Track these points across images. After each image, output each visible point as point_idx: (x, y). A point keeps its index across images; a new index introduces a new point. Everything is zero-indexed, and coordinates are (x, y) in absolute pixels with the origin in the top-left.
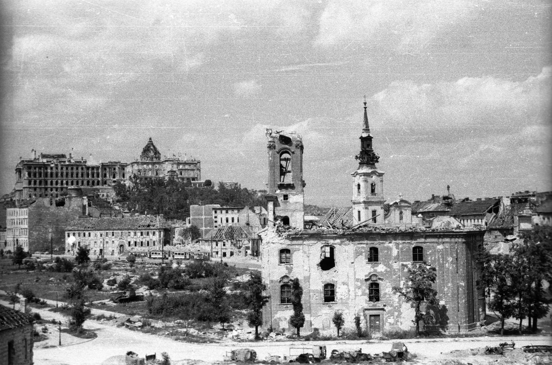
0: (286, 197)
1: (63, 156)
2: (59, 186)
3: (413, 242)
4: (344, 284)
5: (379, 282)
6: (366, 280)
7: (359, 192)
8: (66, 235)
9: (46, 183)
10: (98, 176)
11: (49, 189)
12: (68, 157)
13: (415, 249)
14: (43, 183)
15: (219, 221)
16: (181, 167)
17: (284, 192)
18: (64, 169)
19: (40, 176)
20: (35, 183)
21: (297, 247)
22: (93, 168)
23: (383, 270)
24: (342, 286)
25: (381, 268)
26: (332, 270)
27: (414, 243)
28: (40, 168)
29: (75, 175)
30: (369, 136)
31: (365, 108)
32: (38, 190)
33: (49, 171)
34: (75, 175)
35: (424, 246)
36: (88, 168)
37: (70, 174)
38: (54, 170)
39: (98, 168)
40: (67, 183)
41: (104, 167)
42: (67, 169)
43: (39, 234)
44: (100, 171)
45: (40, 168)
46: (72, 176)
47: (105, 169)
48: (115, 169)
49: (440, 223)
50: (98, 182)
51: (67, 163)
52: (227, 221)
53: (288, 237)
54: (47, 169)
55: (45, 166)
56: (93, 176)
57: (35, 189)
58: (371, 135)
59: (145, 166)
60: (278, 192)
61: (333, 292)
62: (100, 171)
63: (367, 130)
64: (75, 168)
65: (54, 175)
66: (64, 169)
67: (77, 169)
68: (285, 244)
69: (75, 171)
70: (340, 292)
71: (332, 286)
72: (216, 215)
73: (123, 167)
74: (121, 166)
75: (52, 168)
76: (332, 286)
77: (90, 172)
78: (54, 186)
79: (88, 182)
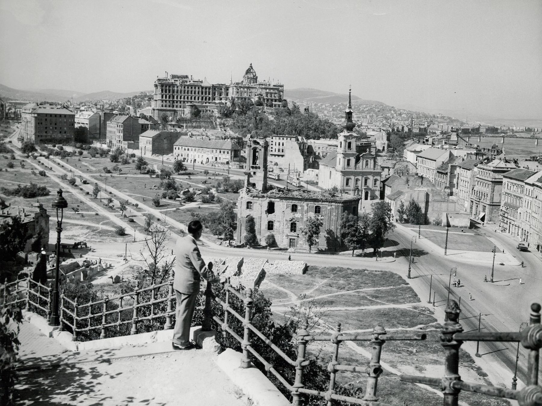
0: (255, 173)
1: (187, 77)
2: (182, 100)
3: (316, 203)
4: (279, 222)
5: (296, 222)
6: (290, 221)
7: (341, 147)
8: (174, 149)
9: (173, 97)
10: (209, 94)
11: (175, 102)
12: (190, 77)
13: (316, 207)
14: (171, 97)
15: (274, 143)
16: (268, 90)
17: (254, 170)
18: (186, 88)
19: (169, 92)
20: (166, 97)
21: (256, 201)
22: (206, 88)
23: (299, 217)
24: (277, 223)
25: (298, 215)
26: (273, 214)
27: (317, 204)
28: (169, 87)
29: (193, 92)
30: (350, 112)
31: (350, 93)
32: (168, 102)
33: (176, 88)
34: (193, 92)
35: (321, 206)
36: (202, 88)
37: (190, 92)
38: (179, 88)
39: (209, 88)
40: (188, 98)
41: (214, 87)
42: (188, 88)
43: (159, 144)
44: (211, 90)
45: (169, 87)
46: (191, 93)
47: (215, 89)
48: (221, 89)
49: (400, 166)
50: (209, 98)
51: (188, 83)
52: (279, 145)
53: (251, 196)
54: (174, 87)
55: (173, 85)
56: (206, 94)
57: (166, 101)
58: (352, 111)
59: (242, 89)
60: (251, 170)
61: (272, 225)
62: (211, 90)
63: (350, 107)
64: (193, 87)
65: (179, 92)
66: (186, 88)
67: (195, 88)
68: (250, 199)
69: (193, 89)
70: (276, 225)
71: (272, 222)
72: (272, 140)
73: (227, 89)
74: (226, 87)
75: (177, 87)
76: (272, 222)
77: (204, 90)
78: (179, 99)
79: (202, 98)
